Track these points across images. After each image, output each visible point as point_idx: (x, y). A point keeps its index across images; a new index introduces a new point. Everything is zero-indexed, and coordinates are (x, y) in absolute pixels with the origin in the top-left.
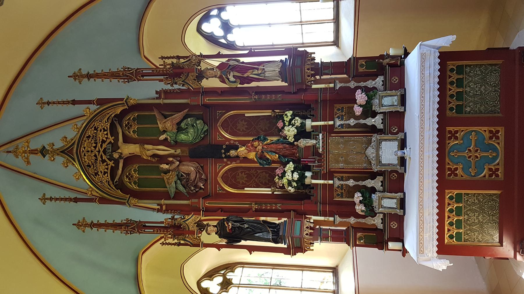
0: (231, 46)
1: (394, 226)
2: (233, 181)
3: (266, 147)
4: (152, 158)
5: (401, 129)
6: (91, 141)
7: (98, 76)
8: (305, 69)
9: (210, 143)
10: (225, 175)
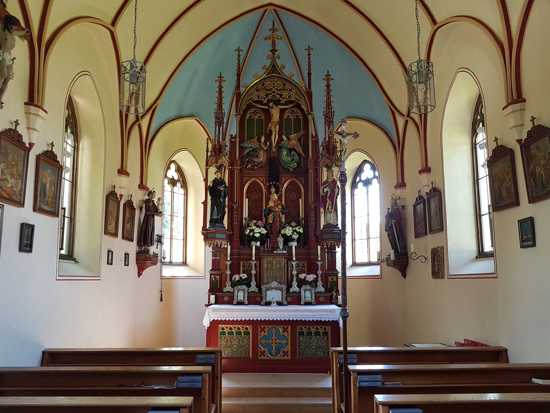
0: (354, 186)
1: (225, 298)
4: (269, 130)
5: (289, 303)
6: (282, 87)
10: (257, 184)
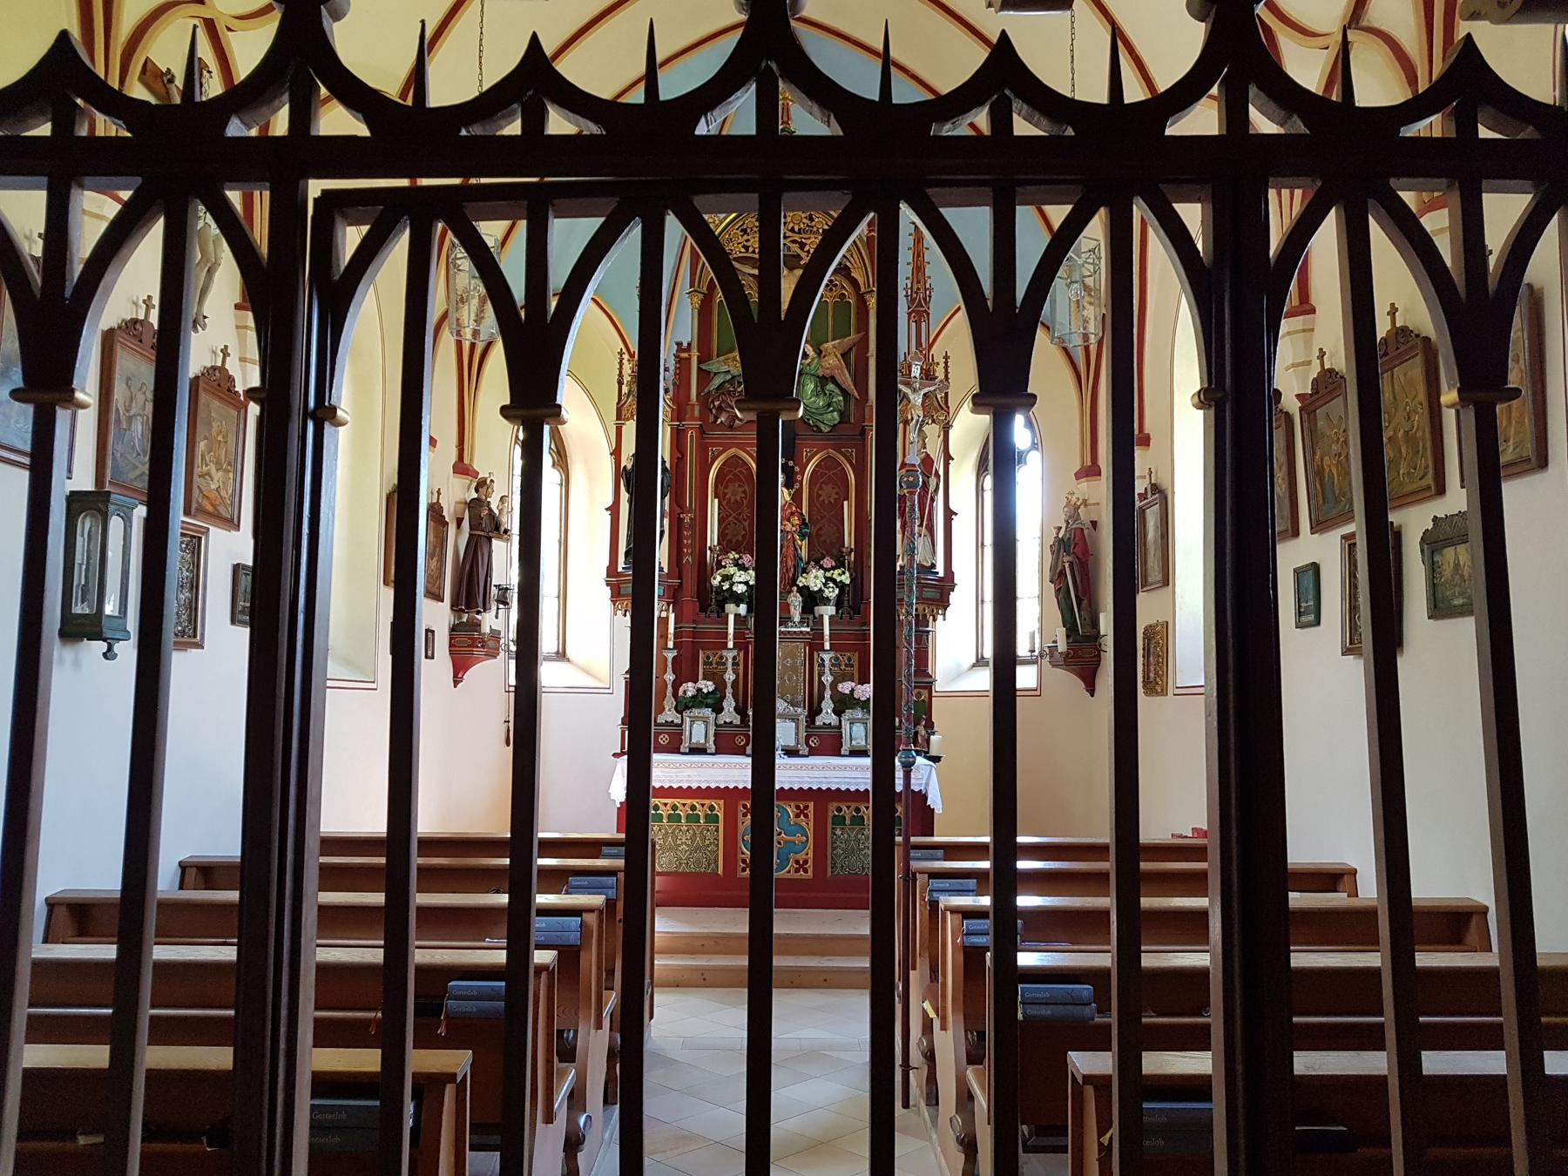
5: (813, 752)
6: (804, 223)
7: (919, 242)
9: (798, 435)
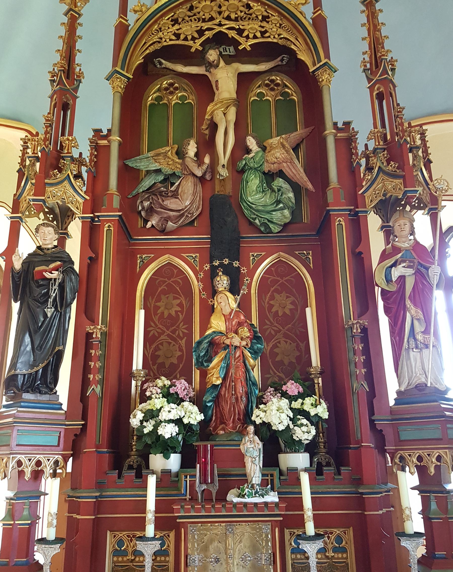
2: (162, 288)
3: (237, 356)
6: (241, 12)
8: (440, 451)
10: (175, 271)
